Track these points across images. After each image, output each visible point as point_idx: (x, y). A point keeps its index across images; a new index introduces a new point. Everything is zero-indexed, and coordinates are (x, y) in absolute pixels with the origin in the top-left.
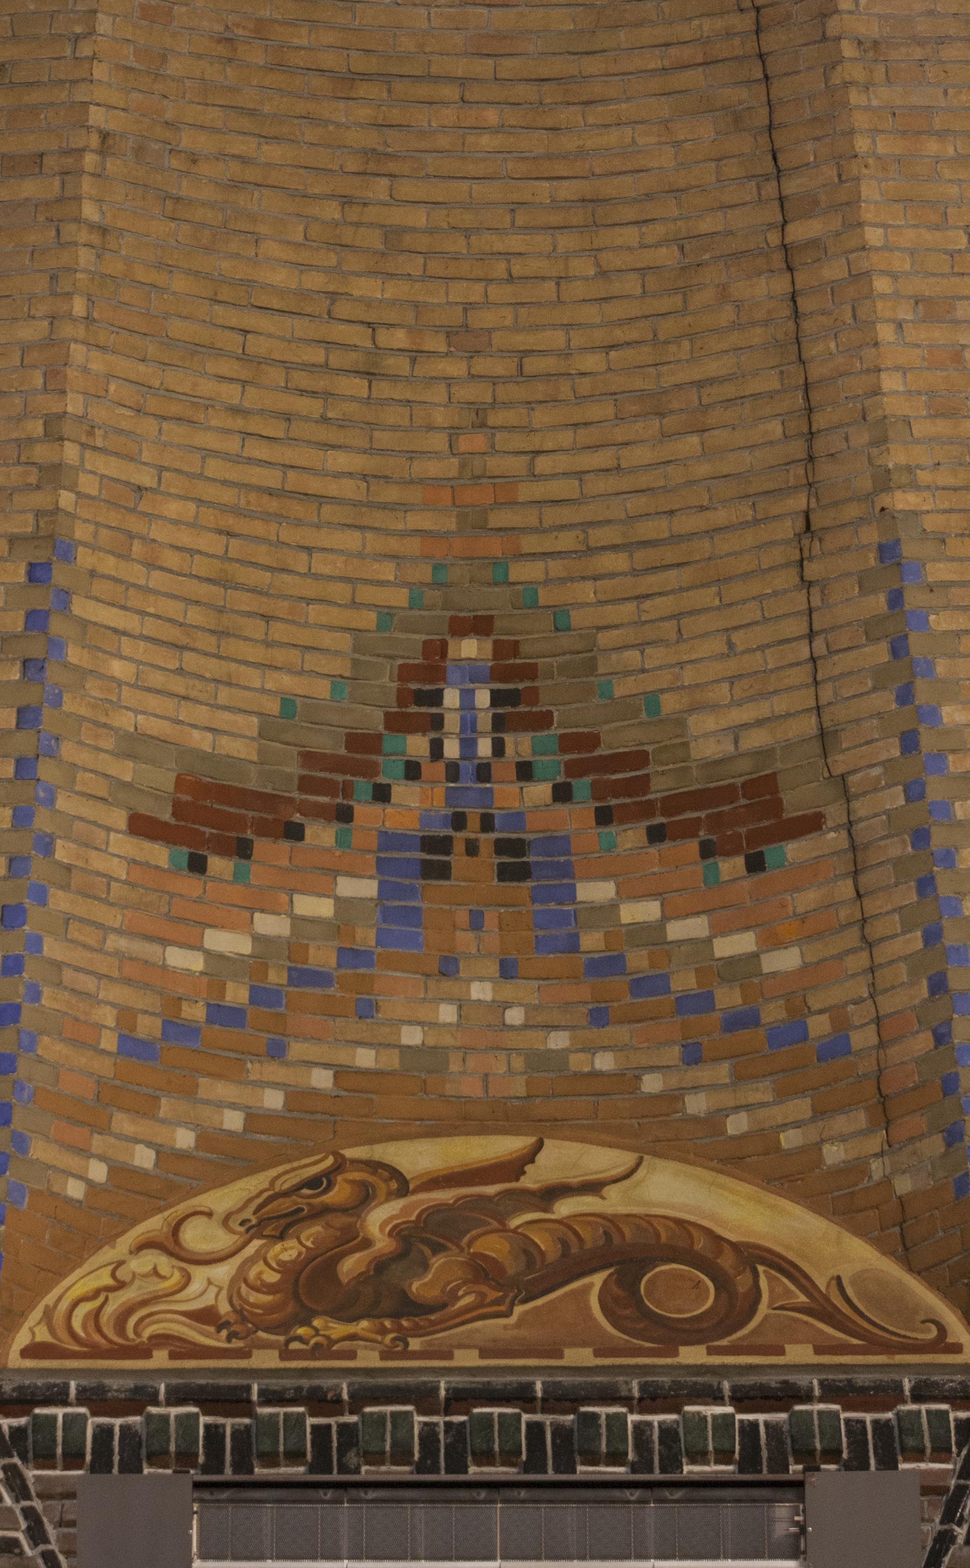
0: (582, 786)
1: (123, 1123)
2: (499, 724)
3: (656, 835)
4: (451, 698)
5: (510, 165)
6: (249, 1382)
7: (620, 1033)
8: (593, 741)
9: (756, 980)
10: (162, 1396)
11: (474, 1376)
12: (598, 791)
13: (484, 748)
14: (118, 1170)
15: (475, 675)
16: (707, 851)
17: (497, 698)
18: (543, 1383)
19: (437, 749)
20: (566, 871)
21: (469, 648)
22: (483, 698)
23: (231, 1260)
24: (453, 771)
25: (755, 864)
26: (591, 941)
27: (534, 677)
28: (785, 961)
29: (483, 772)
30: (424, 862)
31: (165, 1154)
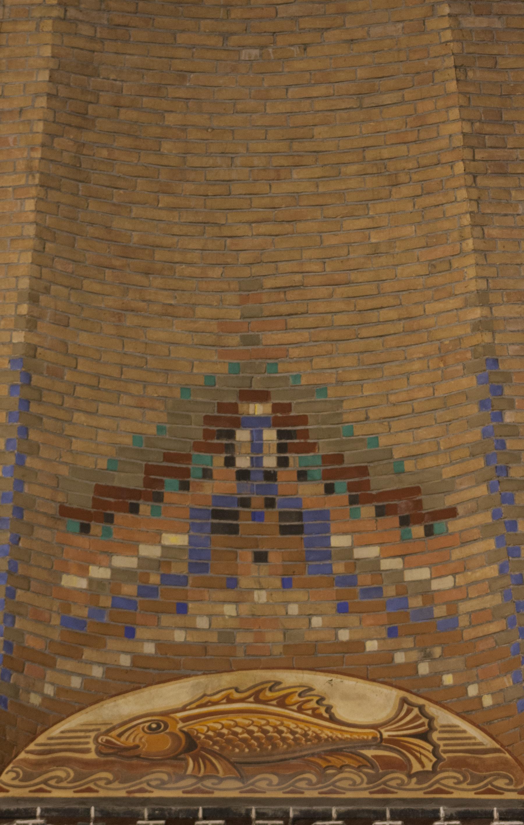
0: (341, 485)
1: (62, 663)
2: (281, 448)
3: (381, 512)
4: (243, 435)
5: (21, 127)
6: (328, 807)
7: (353, 619)
8: (339, 458)
9: (430, 593)
10: (334, 815)
11: (311, 805)
12: (351, 487)
13: (270, 462)
14: (60, 690)
15: (261, 422)
16: (405, 521)
17: (281, 435)
18: (204, 810)
19: (230, 462)
20: (326, 529)
21: (258, 409)
22: (270, 435)
23: (494, 742)
24: (243, 475)
25: (429, 532)
26: (339, 568)
27: (306, 423)
28: (447, 583)
29: (270, 476)
30: (213, 524)
31: (88, 680)
